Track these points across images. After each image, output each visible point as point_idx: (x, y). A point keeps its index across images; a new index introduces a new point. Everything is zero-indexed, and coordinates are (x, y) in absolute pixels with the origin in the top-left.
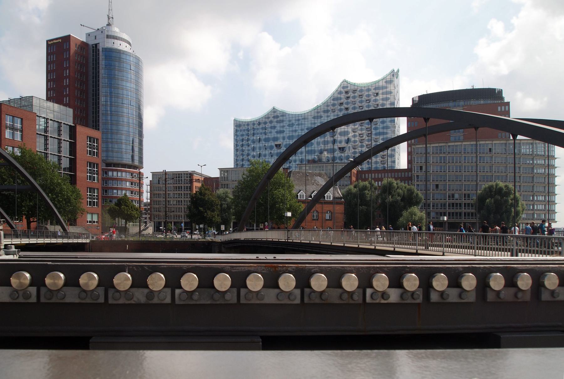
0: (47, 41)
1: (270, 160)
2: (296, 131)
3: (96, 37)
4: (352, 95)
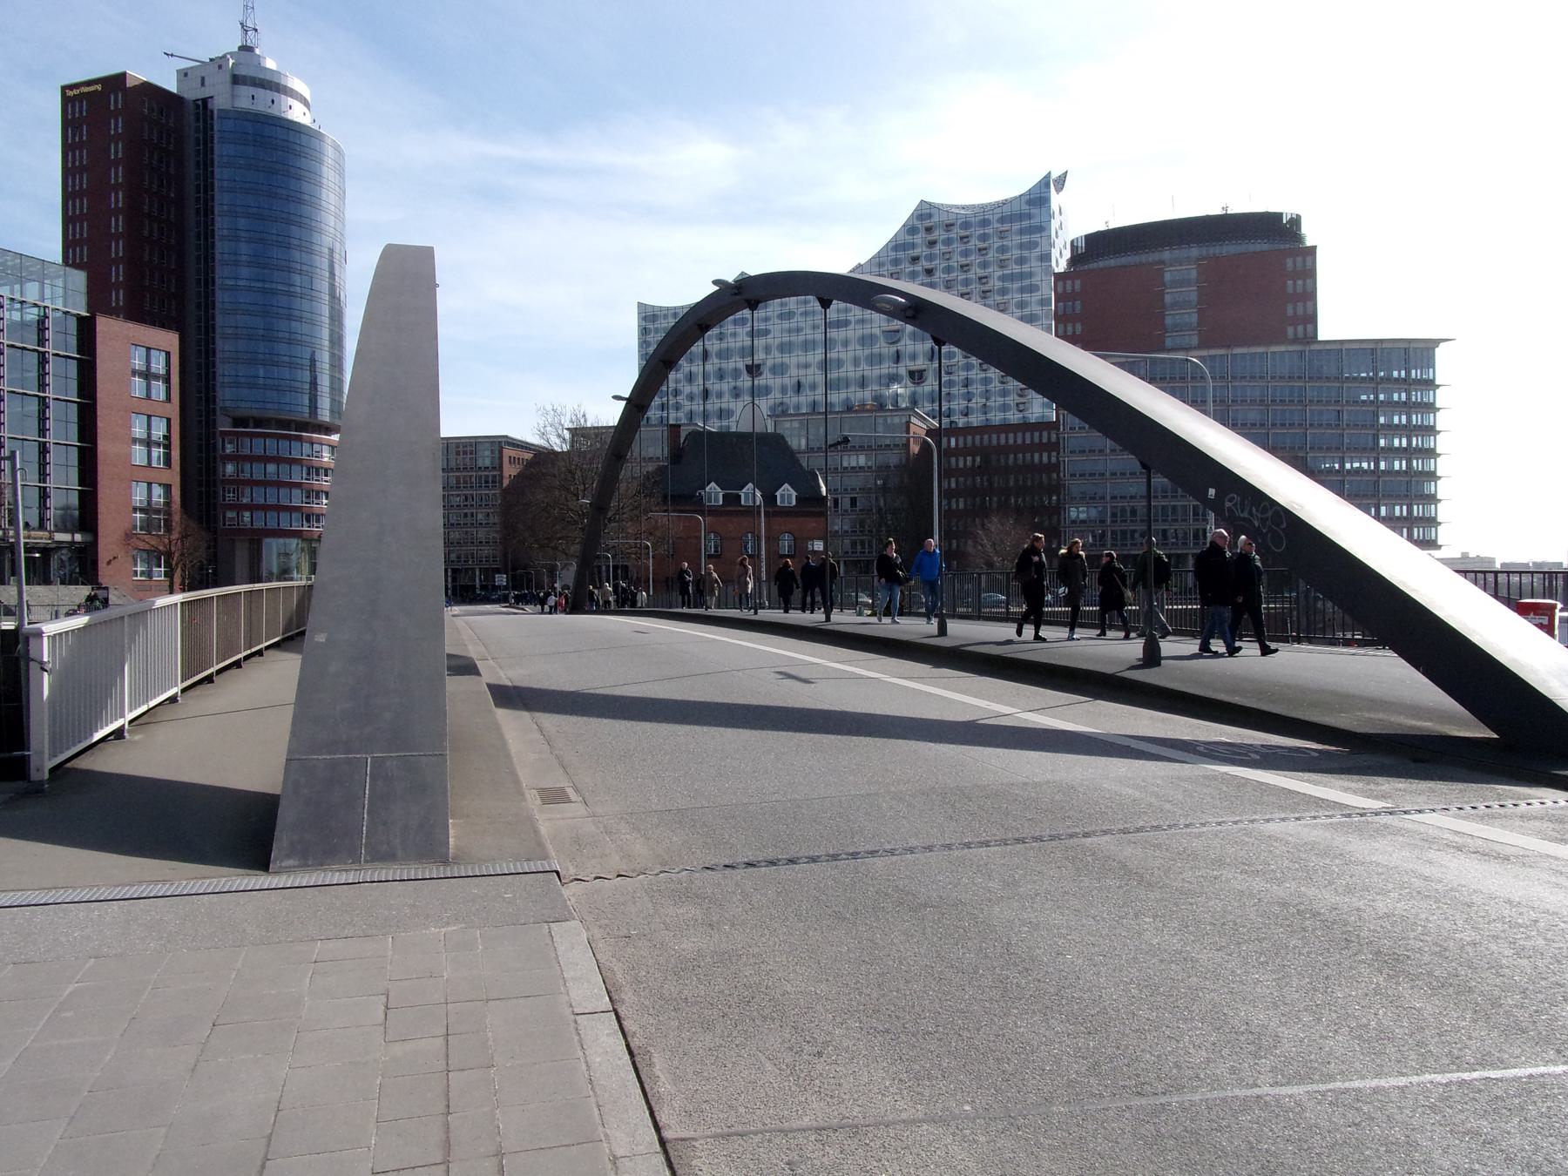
0: (64, 89)
1: (732, 406)
2: (798, 330)
3: (203, 79)
4: (944, 236)
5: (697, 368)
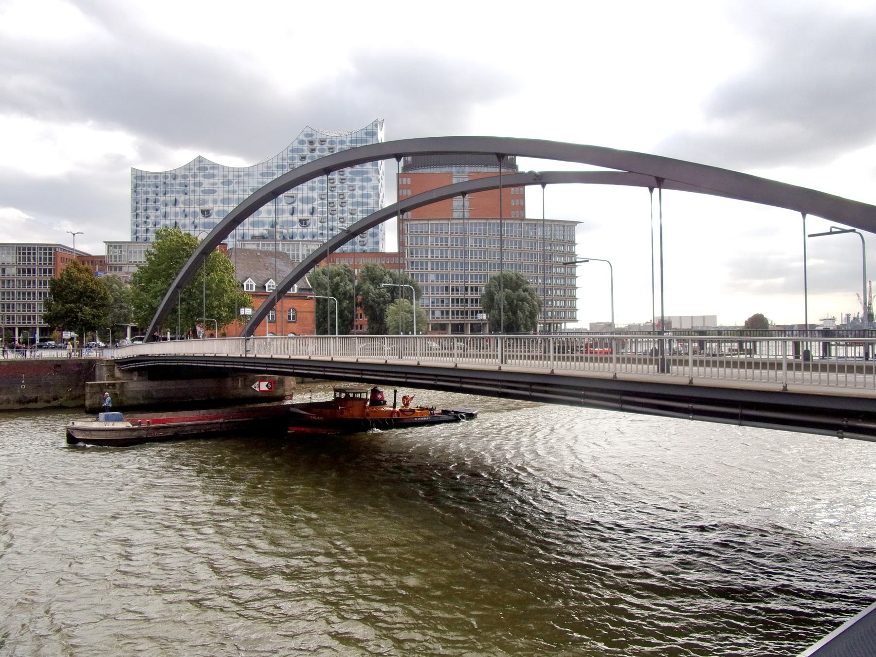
2: (234, 192)
5: (337, 224)
